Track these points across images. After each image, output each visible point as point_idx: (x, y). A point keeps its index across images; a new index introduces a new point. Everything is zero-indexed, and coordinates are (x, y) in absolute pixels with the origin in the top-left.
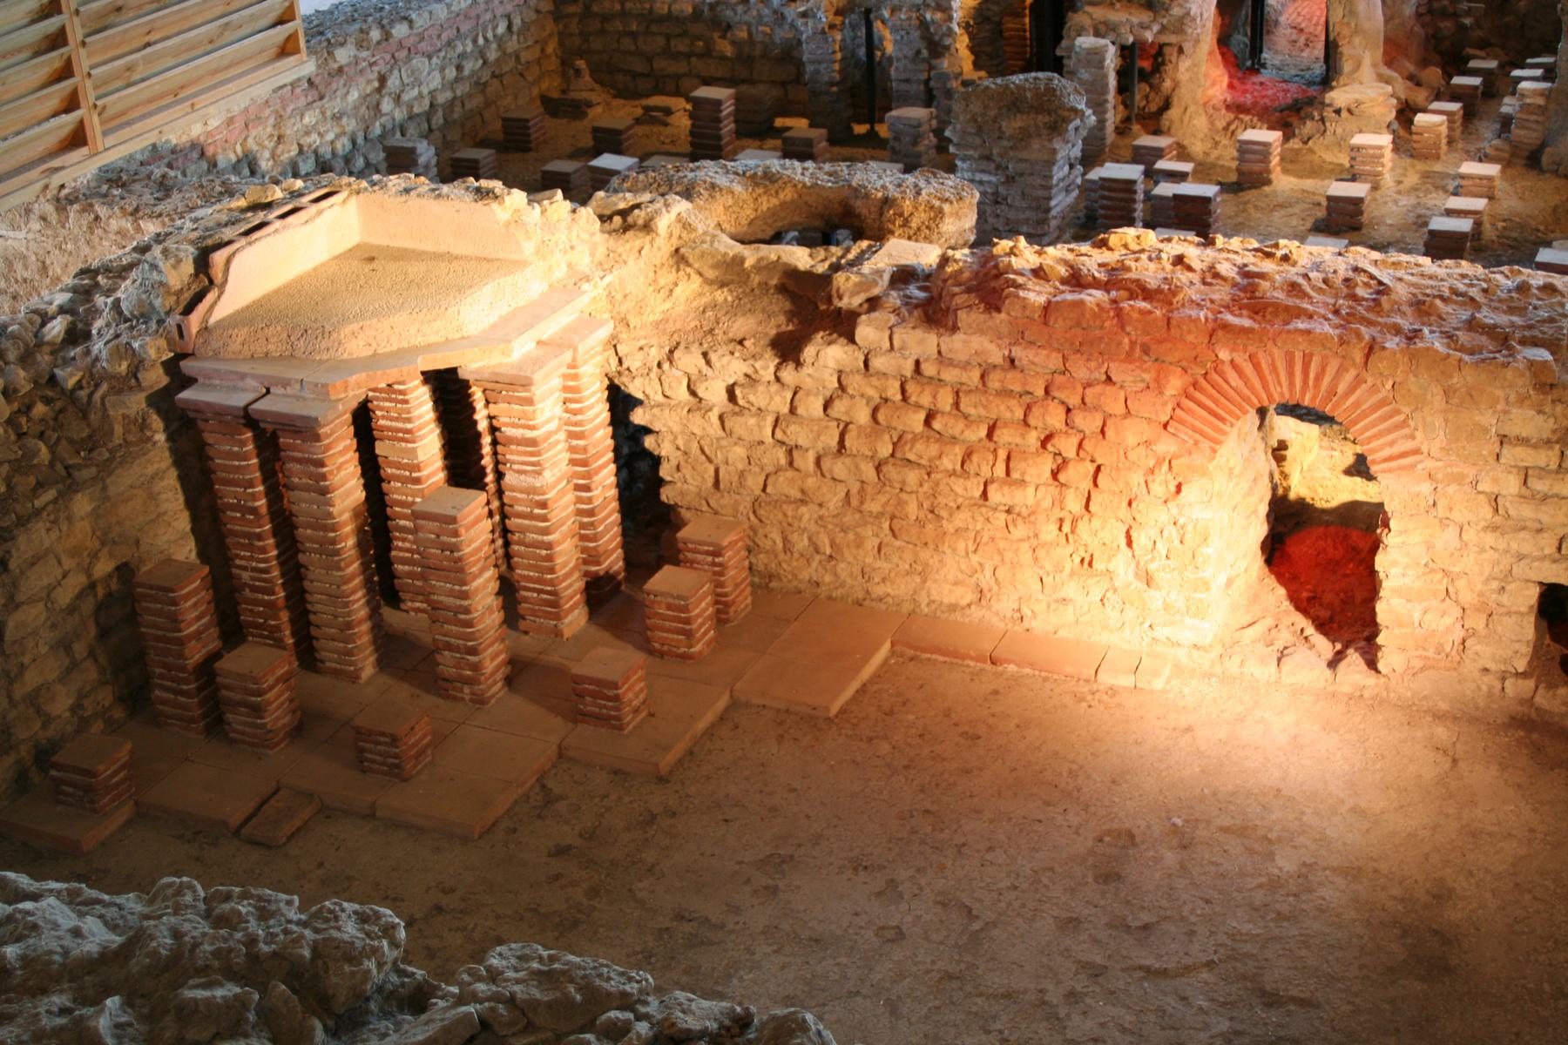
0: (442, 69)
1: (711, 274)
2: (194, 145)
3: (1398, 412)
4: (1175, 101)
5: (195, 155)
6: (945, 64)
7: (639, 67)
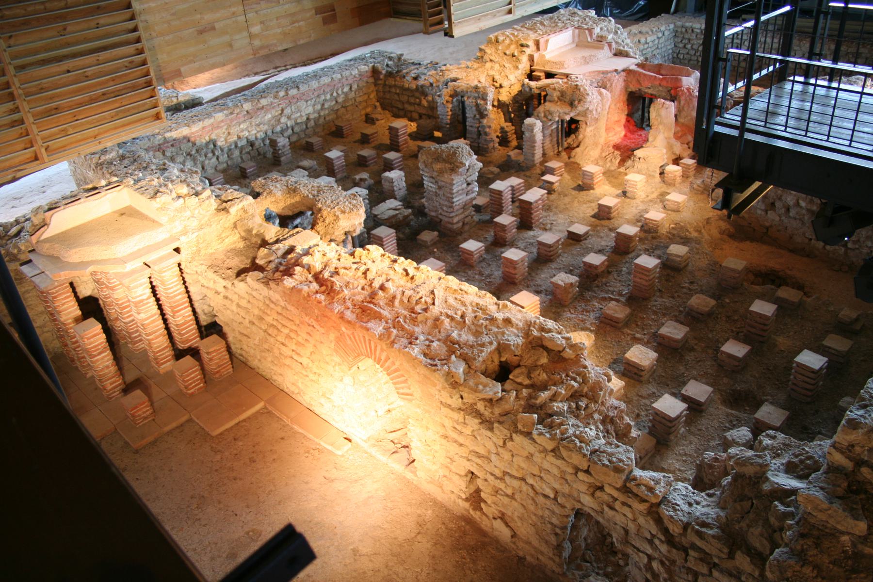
0: (314, 105)
1: (243, 234)
2: (185, 137)
3: (403, 376)
4: (582, 145)
5: (185, 141)
6: (485, 121)
7: (400, 106)
